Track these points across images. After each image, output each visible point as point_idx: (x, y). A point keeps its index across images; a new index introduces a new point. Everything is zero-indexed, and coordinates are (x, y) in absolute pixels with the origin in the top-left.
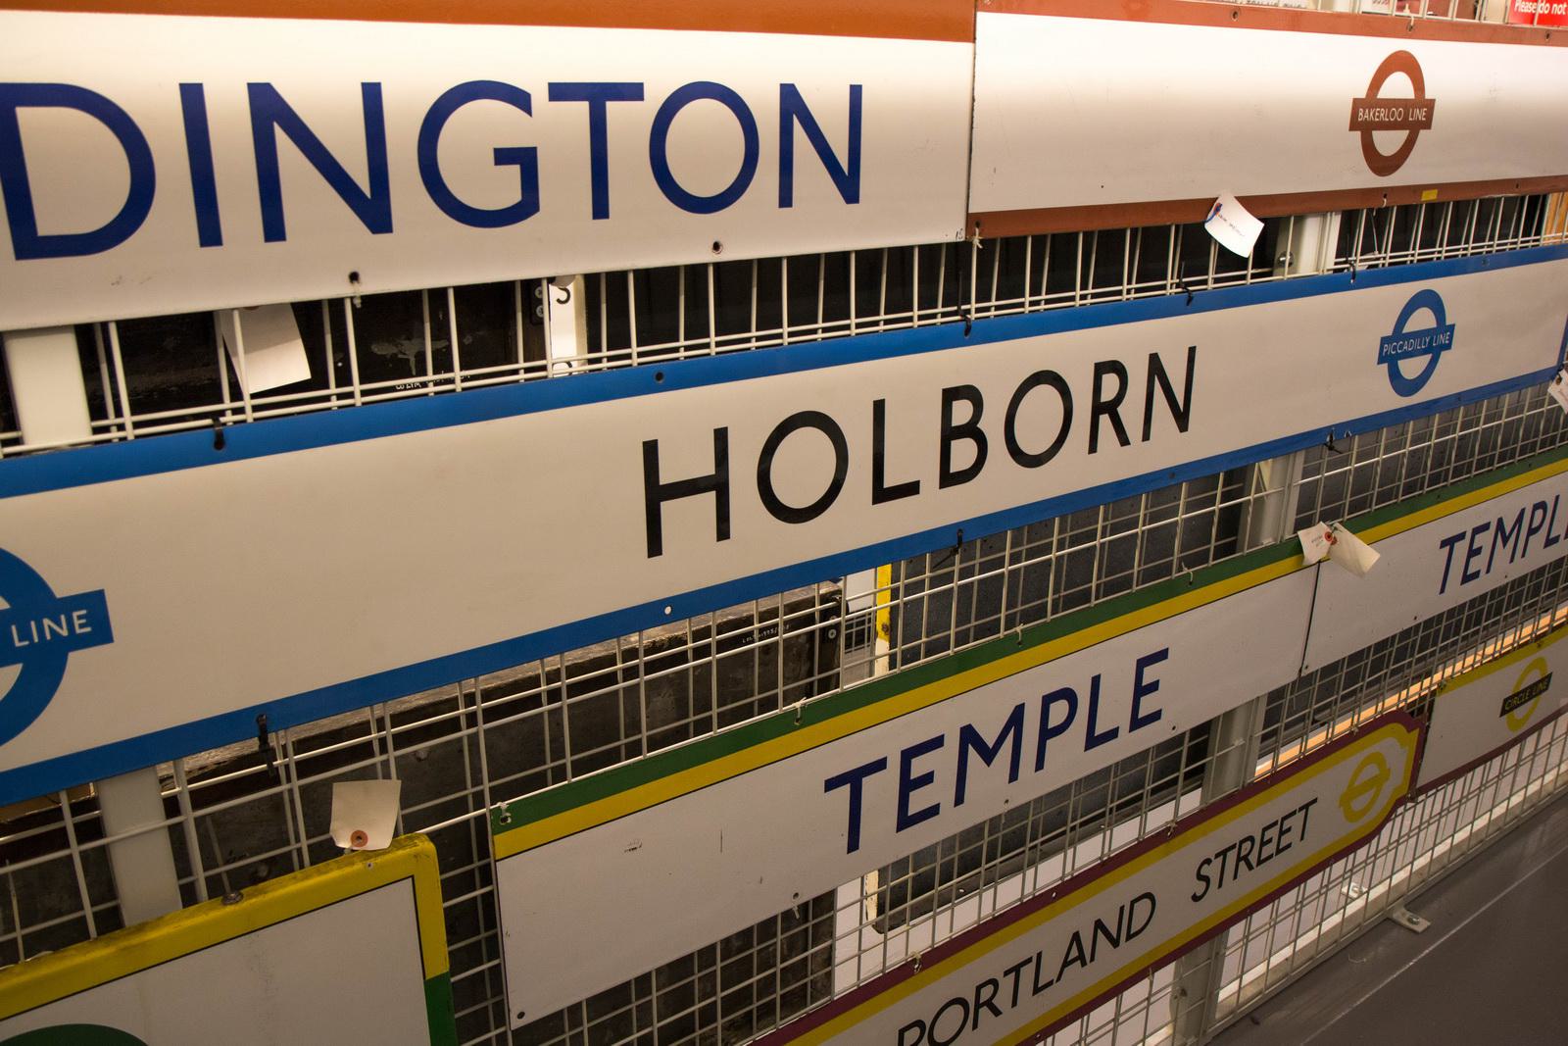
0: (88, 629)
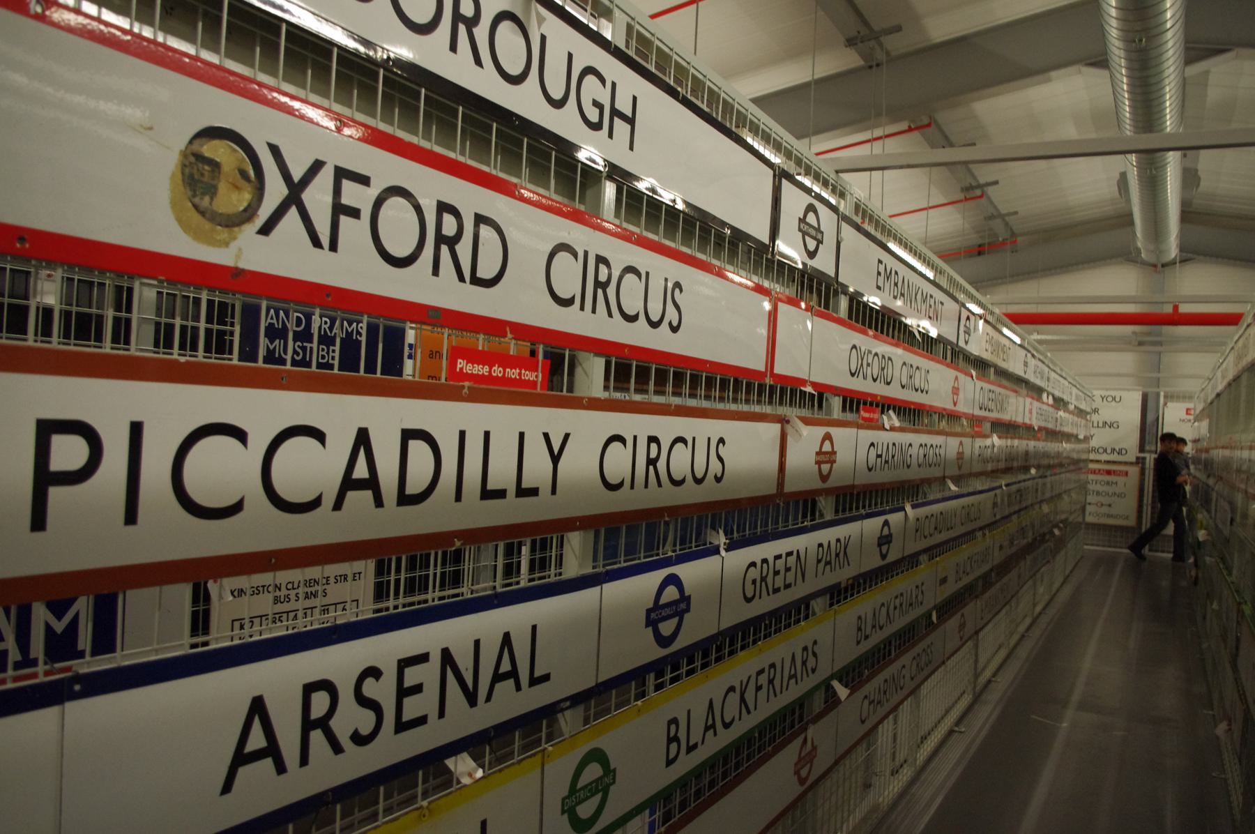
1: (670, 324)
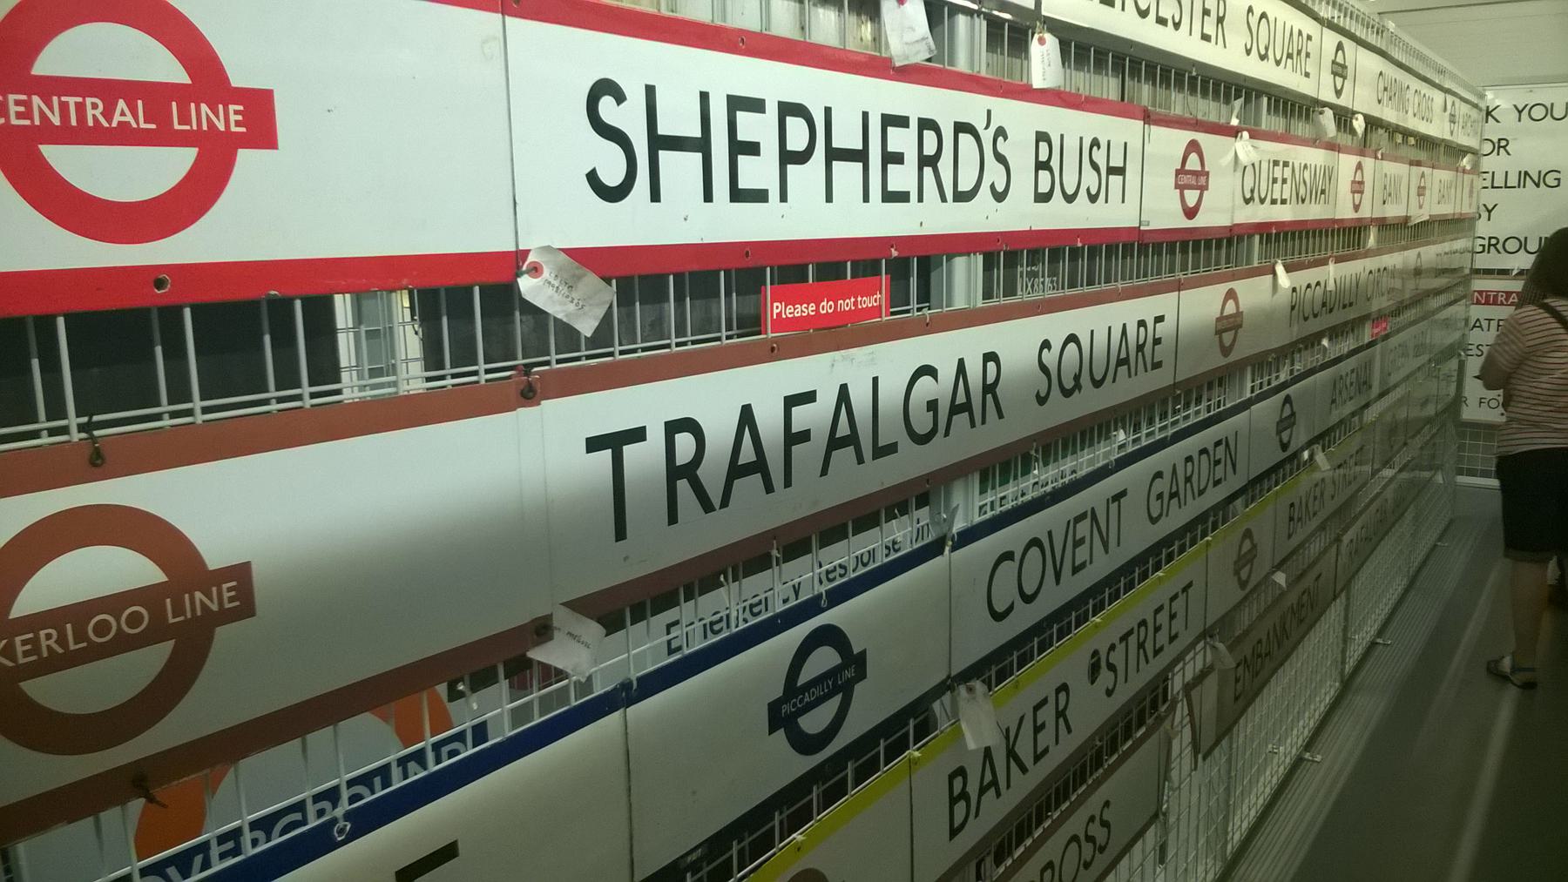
0: (243, 130)
1: (992, 187)
